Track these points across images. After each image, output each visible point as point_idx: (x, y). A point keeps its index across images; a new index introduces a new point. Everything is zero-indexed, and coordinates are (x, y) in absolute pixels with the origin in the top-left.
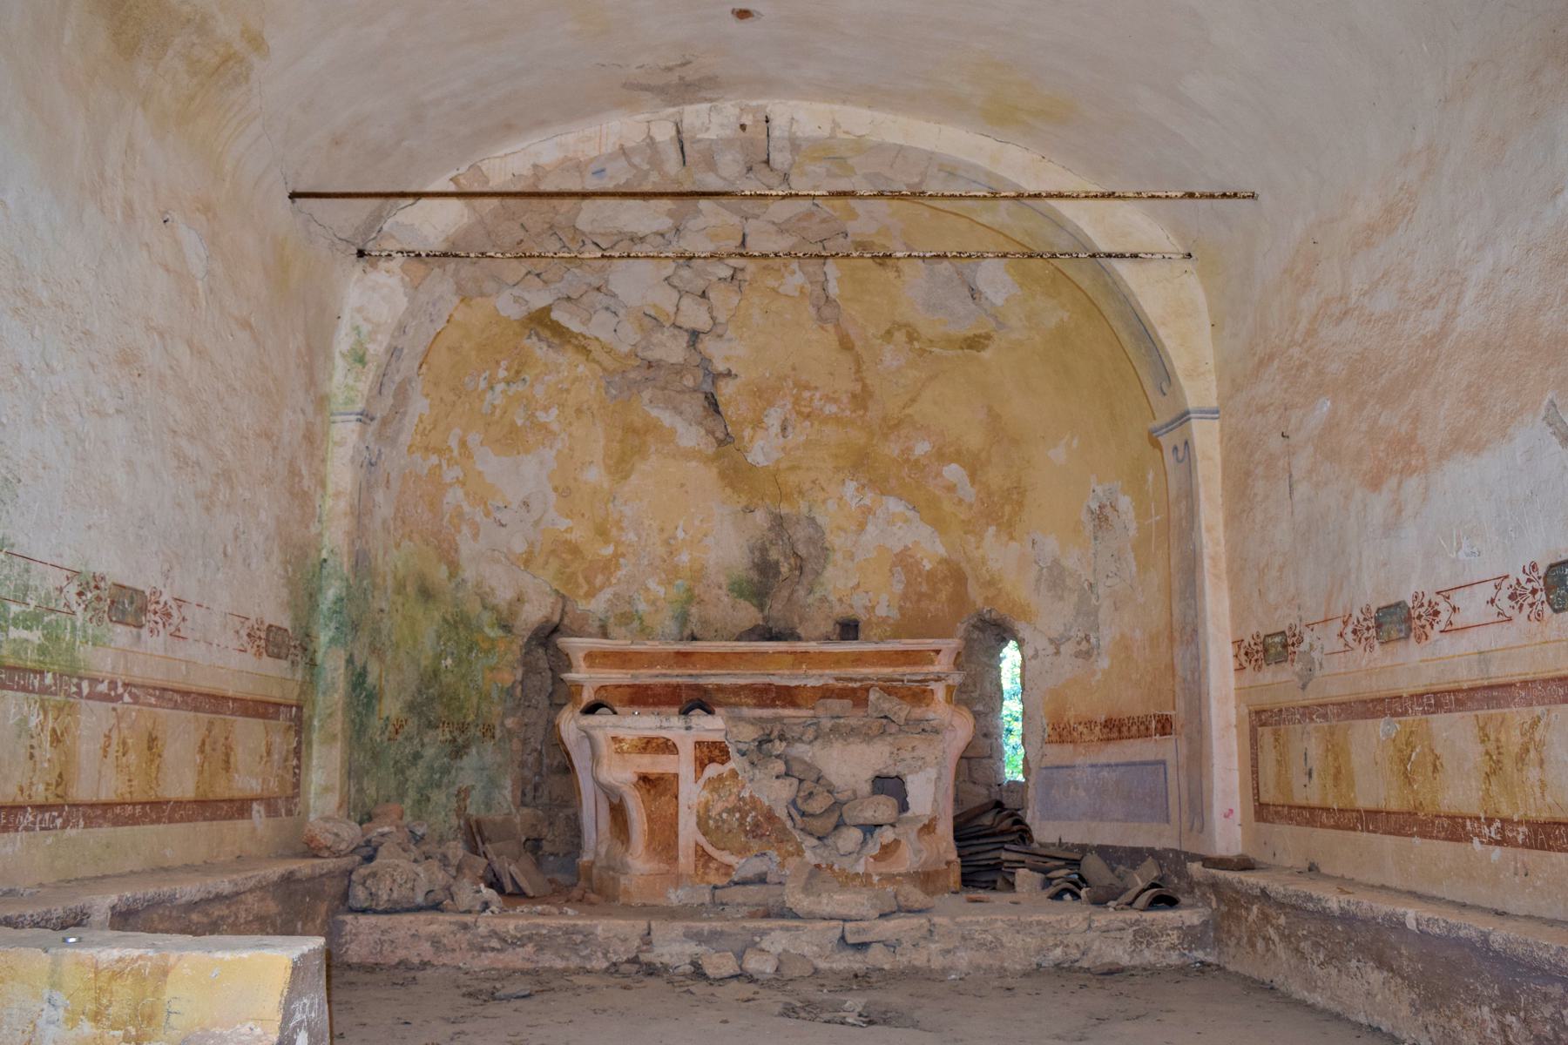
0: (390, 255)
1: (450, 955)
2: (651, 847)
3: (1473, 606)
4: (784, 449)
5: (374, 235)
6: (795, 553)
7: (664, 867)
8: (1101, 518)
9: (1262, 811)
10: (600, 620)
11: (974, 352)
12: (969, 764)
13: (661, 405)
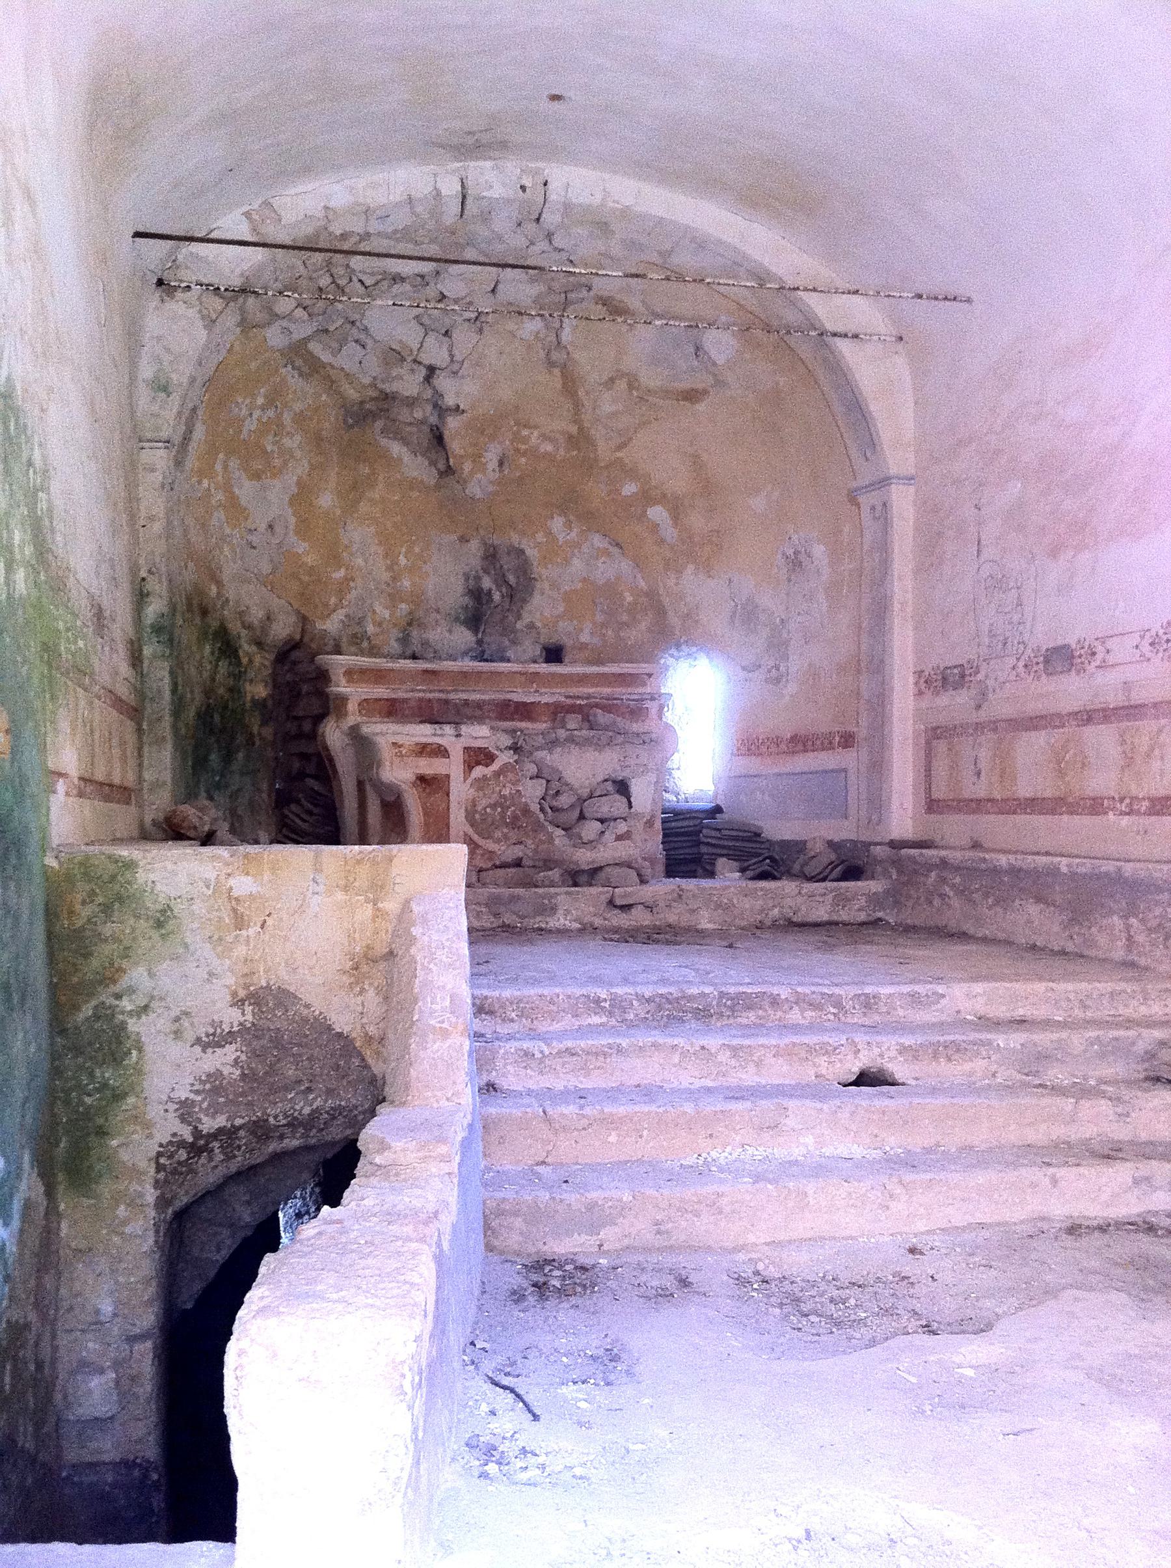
0: (188, 287)
3: (1122, 650)
8: (796, 563)
9: (933, 806)
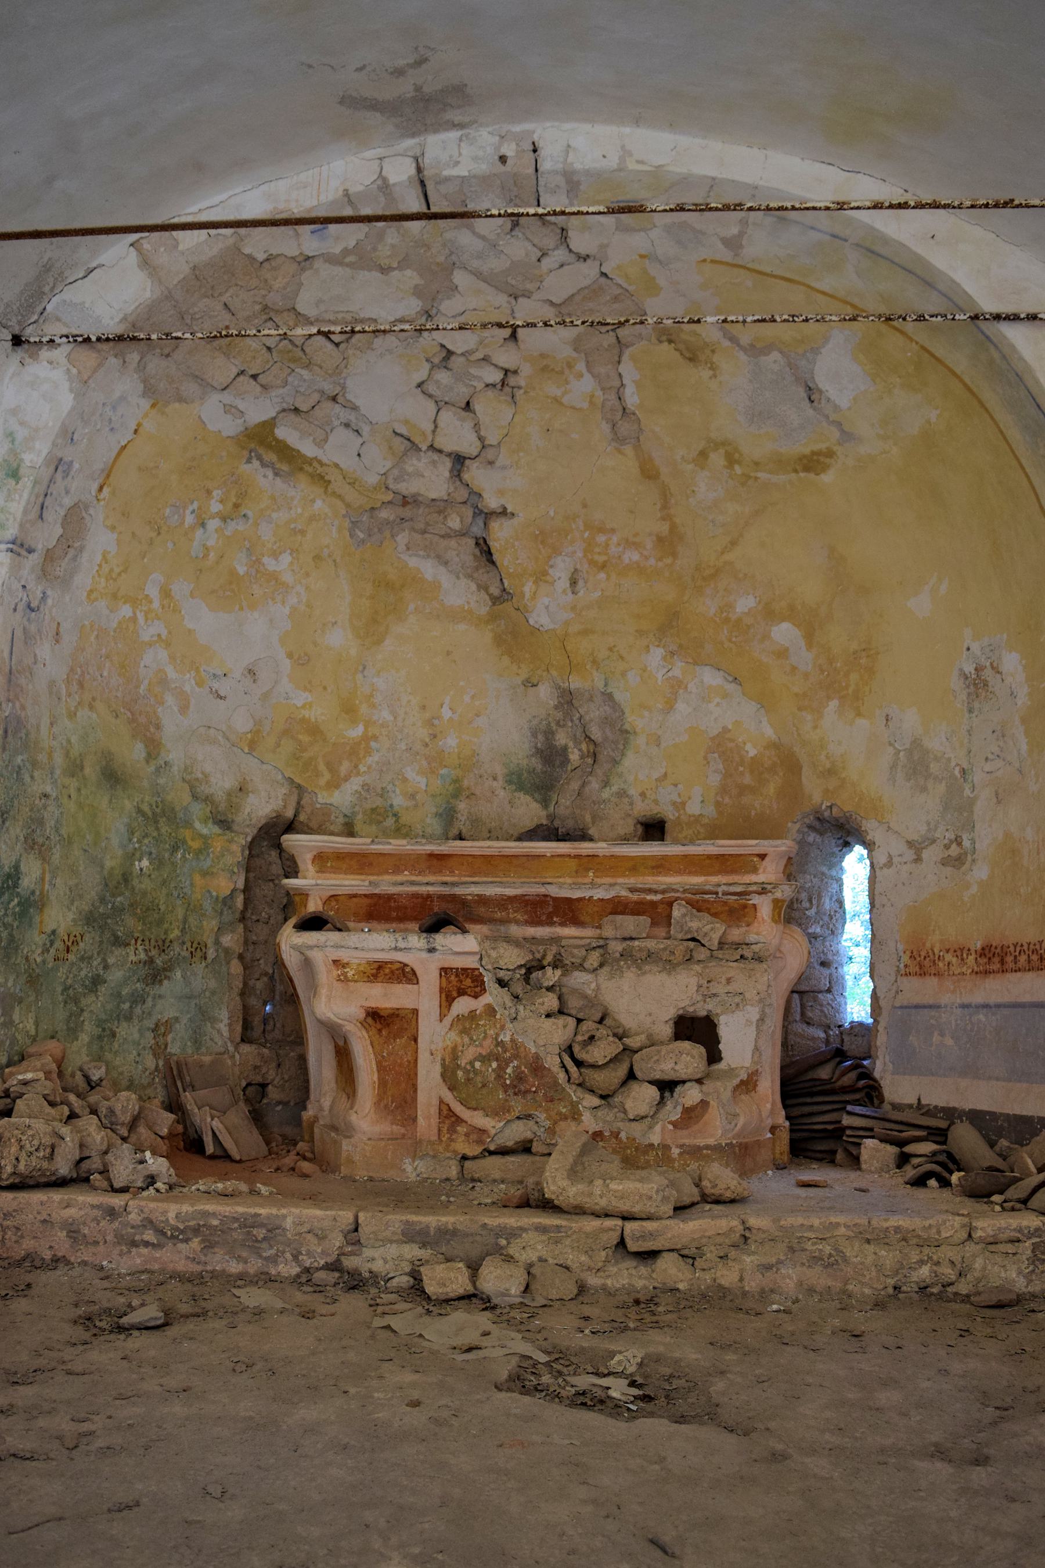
0: (52, 341)
1: (92, 1249)
2: (382, 1105)
4: (573, 608)
5: (36, 317)
6: (587, 736)
7: (398, 1130)
10: (345, 816)
11: (812, 476)
12: (801, 1000)
13: (421, 553)
